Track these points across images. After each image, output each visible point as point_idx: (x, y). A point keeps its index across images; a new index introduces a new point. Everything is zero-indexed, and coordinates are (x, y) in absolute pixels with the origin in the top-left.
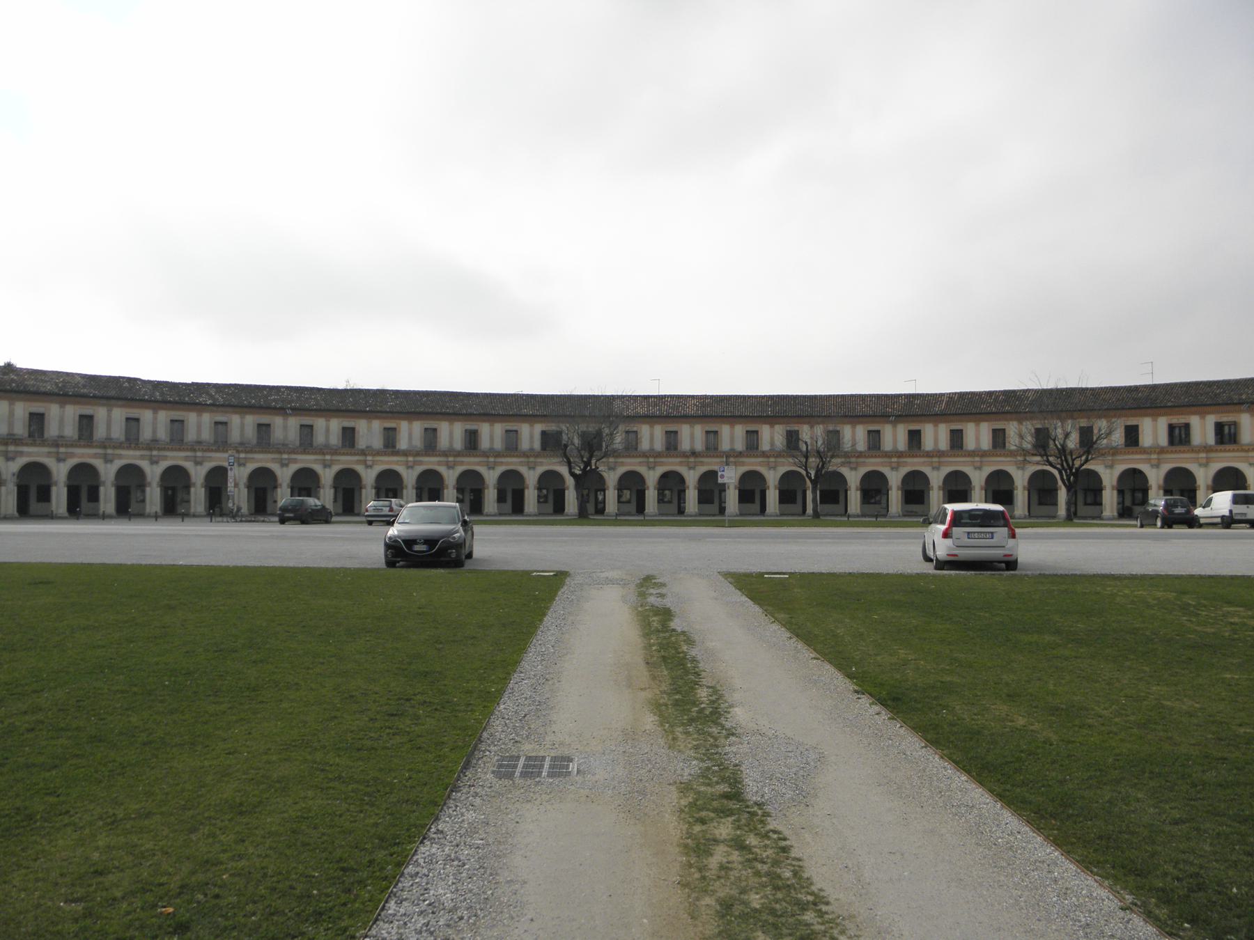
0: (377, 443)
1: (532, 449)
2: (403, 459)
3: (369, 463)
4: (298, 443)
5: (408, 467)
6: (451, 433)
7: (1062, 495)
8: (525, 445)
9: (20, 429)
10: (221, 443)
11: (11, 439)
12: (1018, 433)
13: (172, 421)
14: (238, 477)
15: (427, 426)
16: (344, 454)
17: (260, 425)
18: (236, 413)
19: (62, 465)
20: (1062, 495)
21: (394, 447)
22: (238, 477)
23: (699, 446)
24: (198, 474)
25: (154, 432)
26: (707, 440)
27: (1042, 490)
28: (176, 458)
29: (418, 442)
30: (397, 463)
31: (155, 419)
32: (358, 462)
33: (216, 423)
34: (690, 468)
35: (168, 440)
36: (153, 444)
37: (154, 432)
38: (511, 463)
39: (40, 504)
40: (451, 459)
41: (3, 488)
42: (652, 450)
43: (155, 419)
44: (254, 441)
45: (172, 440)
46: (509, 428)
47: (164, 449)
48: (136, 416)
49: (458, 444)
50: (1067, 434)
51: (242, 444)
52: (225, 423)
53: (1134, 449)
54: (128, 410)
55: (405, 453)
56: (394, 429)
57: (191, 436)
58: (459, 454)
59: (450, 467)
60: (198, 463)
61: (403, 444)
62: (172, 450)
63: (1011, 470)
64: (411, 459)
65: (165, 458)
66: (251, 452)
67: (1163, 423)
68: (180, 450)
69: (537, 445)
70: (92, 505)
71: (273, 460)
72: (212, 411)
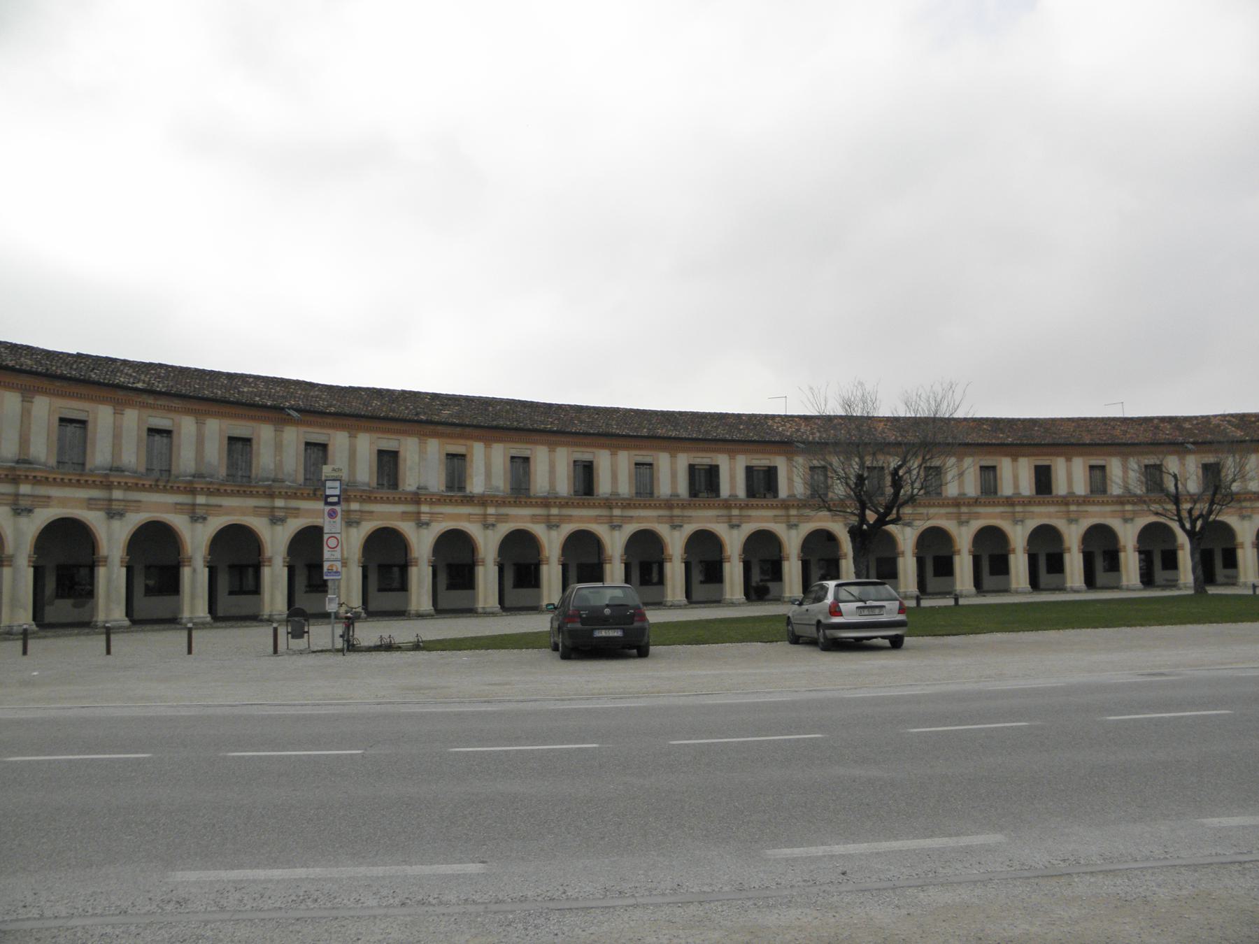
0: (436, 481)
1: (675, 495)
2: (477, 510)
3: (424, 518)
4: (301, 479)
5: (486, 526)
6: (552, 468)
7: (1185, 558)
8: (664, 488)
9: (41, 449)
10: (160, 476)
11: (19, 471)
12: (1123, 474)
13: (63, 421)
14: (343, 552)
15: (515, 453)
16: (382, 501)
17: (232, 440)
18: (188, 412)
19: (116, 524)
20: (1185, 558)
21: (462, 488)
22: (343, 552)
23: (131, 456)
24: (276, 541)
25: (24, 441)
26: (61, 439)
27: (1157, 554)
28: (237, 510)
29: (501, 483)
30: (469, 517)
31: (26, 415)
32: (404, 516)
33: (152, 431)
34: (732, 527)
35: (53, 462)
36: (110, 477)
37: (24, 441)
38: (645, 519)
39: (995, 578)
40: (554, 511)
41: (7, 571)
42: (792, 496)
43: (26, 415)
44: (223, 472)
45: (60, 463)
46: (640, 459)
47: (45, 481)
48: (648, 460)
49: (564, 487)
50: (1186, 472)
51: (198, 475)
52: (168, 433)
53: (1047, 498)
54: (692, 455)
55: (483, 501)
56: (463, 456)
57: (100, 455)
58: (565, 503)
59: (551, 525)
60: (275, 520)
61: (476, 485)
62: (62, 483)
63: (1115, 524)
64: (491, 510)
65: (569, 519)
66: (218, 493)
67: (683, 460)
68: (78, 484)
69: (683, 489)
70: (1229, 572)
71: (257, 511)
72: (144, 406)
